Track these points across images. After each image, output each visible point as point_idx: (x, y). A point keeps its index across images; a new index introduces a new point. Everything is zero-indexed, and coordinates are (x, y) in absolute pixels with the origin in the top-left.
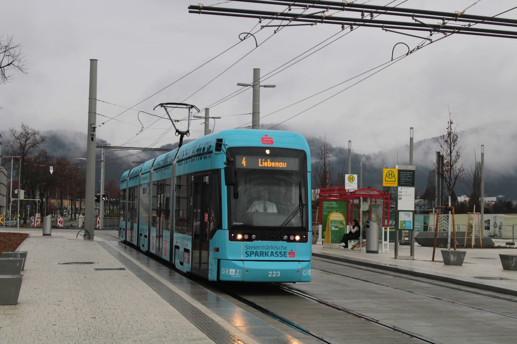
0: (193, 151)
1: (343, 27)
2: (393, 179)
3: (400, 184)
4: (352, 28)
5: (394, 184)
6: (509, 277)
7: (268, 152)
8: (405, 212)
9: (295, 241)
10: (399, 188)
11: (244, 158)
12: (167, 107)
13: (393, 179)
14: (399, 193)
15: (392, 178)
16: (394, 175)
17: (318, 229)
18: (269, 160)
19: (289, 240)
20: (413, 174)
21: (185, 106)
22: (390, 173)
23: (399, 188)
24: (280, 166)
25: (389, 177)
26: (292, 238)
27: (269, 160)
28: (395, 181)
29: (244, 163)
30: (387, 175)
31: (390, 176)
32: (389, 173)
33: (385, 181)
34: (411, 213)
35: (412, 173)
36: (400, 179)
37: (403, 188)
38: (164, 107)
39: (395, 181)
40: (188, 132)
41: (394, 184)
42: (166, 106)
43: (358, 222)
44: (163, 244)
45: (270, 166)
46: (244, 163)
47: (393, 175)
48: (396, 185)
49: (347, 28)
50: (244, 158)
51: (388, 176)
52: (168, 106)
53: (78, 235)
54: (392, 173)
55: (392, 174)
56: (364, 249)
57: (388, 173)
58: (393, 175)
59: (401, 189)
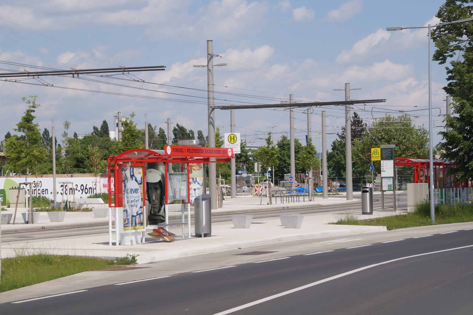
2: (378, 155)
3: (382, 159)
10: (382, 162)
16: (378, 153)
22: (376, 151)
23: (382, 162)
28: (379, 157)
30: (373, 153)
31: (376, 153)
34: (392, 179)
37: (384, 161)
39: (379, 157)
48: (380, 159)
55: (376, 152)
57: (230, 137)
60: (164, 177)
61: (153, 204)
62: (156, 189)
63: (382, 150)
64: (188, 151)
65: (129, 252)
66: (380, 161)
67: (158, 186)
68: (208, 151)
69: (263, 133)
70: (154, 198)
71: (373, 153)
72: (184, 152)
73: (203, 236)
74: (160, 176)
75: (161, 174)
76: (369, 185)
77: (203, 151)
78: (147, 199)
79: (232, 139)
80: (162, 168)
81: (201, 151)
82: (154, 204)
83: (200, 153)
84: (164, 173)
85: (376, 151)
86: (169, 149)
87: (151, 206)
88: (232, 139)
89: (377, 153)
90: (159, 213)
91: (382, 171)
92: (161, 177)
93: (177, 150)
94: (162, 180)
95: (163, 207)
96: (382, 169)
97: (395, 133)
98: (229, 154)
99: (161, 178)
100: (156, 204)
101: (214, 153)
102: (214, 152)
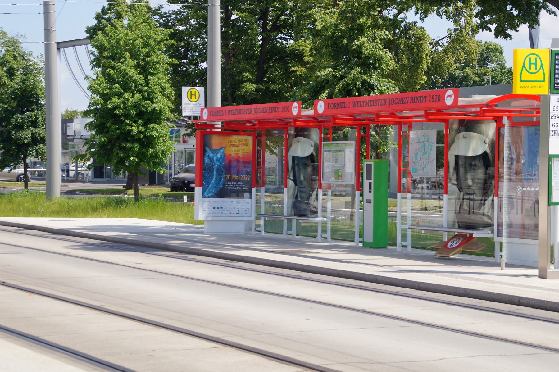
2: (539, 76)
5: (541, 87)
6: (72, 219)
13: (539, 76)
15: (537, 72)
16: (542, 66)
17: (442, 238)
22: (533, 61)
25: (536, 57)
28: (544, 81)
30: (524, 66)
31: (533, 66)
32: (530, 59)
33: (521, 81)
39: (544, 81)
41: (541, 87)
44: (536, 211)
51: (527, 68)
53: (469, 201)
54: (536, 59)
55: (536, 64)
57: (527, 59)
60: (318, 149)
61: (299, 186)
62: (306, 166)
64: (229, 113)
66: (547, 99)
67: (479, 163)
68: (259, 110)
70: (302, 178)
71: (524, 66)
72: (224, 114)
73: (503, 265)
74: (313, 147)
75: (313, 144)
77: (251, 111)
78: (292, 178)
79: (193, 95)
80: (490, 129)
81: (247, 111)
82: (301, 186)
83: (379, 105)
84: (318, 142)
85: (533, 61)
86: (205, 113)
87: (298, 189)
88: (192, 96)
89: (538, 68)
90: (308, 201)
91: (551, 133)
92: (313, 148)
93: (215, 113)
94: (314, 153)
95: (315, 192)
96: (551, 128)
98: (293, 111)
99: (314, 150)
100: (305, 187)
101: (268, 112)
102: (268, 110)
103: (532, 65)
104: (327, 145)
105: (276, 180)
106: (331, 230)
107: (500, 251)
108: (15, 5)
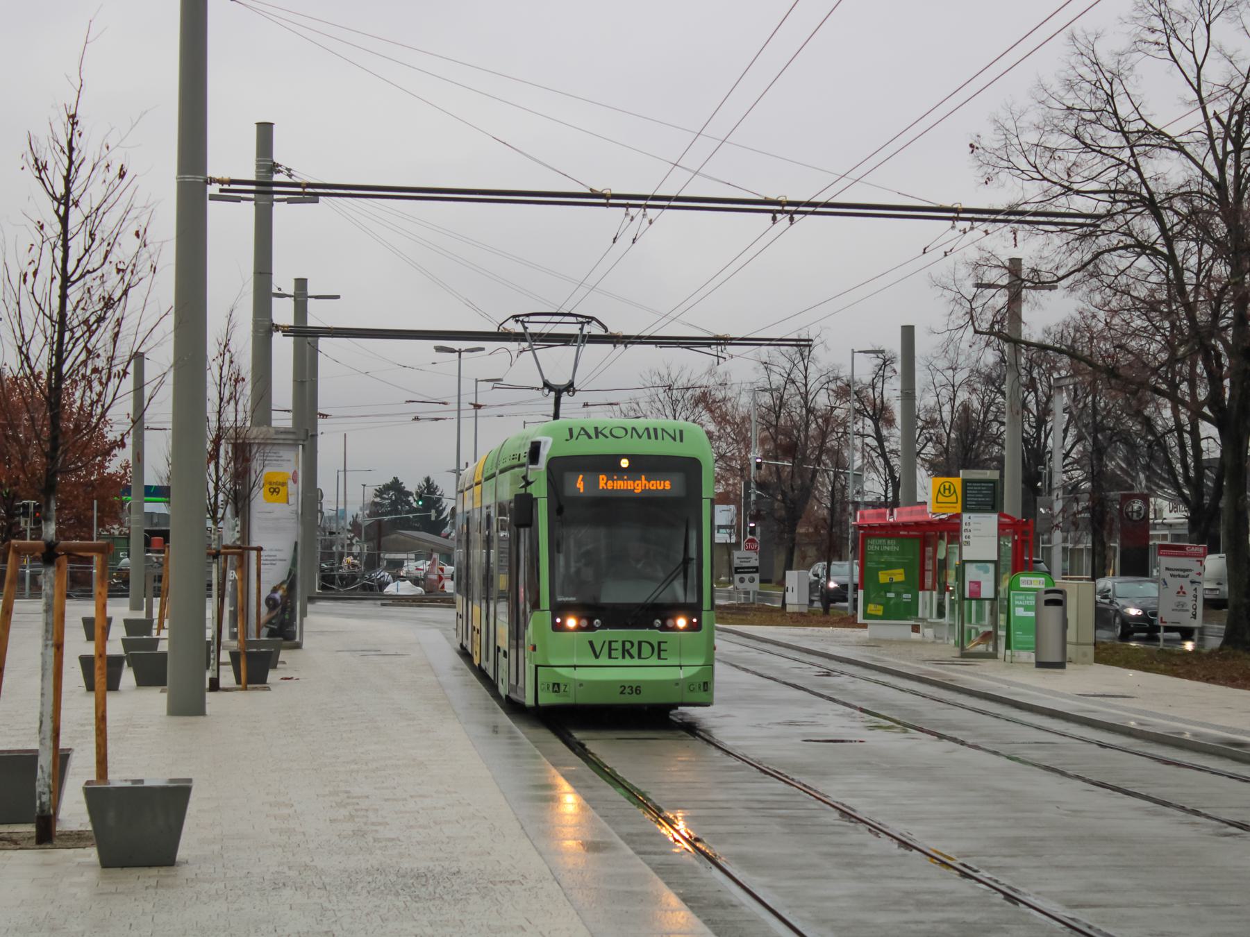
0: (592, 434)
1: (774, 219)
2: (953, 498)
3: (966, 508)
4: (792, 220)
5: (955, 507)
7: (625, 463)
8: (979, 564)
9: (675, 629)
10: (965, 517)
11: (581, 476)
12: (528, 322)
14: (964, 527)
16: (955, 491)
18: (643, 477)
19: (664, 628)
20: (994, 487)
21: (573, 319)
22: (947, 487)
23: (965, 517)
24: (652, 488)
26: (670, 623)
27: (643, 477)
28: (957, 502)
29: (580, 485)
31: (947, 491)
34: (991, 567)
35: (992, 485)
36: (966, 501)
37: (972, 515)
38: (523, 322)
39: (957, 502)
40: (571, 384)
41: (955, 507)
42: (526, 319)
43: (285, 586)
45: (652, 482)
46: (580, 485)
47: (952, 491)
48: (958, 510)
49: (783, 220)
50: (581, 476)
52: (532, 318)
55: (949, 489)
56: (1028, 656)
57: (942, 486)
58: (952, 491)
59: (970, 518)
63: (965, 483)
65: (1023, 267)
69: (283, 348)
76: (892, 514)
85: (947, 487)
97: (1147, 345)
103: (215, 210)
104: (297, 456)
105: (156, 526)
106: (653, 869)
107: (912, 328)
108: (337, 297)
